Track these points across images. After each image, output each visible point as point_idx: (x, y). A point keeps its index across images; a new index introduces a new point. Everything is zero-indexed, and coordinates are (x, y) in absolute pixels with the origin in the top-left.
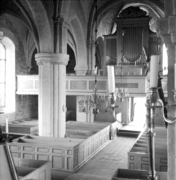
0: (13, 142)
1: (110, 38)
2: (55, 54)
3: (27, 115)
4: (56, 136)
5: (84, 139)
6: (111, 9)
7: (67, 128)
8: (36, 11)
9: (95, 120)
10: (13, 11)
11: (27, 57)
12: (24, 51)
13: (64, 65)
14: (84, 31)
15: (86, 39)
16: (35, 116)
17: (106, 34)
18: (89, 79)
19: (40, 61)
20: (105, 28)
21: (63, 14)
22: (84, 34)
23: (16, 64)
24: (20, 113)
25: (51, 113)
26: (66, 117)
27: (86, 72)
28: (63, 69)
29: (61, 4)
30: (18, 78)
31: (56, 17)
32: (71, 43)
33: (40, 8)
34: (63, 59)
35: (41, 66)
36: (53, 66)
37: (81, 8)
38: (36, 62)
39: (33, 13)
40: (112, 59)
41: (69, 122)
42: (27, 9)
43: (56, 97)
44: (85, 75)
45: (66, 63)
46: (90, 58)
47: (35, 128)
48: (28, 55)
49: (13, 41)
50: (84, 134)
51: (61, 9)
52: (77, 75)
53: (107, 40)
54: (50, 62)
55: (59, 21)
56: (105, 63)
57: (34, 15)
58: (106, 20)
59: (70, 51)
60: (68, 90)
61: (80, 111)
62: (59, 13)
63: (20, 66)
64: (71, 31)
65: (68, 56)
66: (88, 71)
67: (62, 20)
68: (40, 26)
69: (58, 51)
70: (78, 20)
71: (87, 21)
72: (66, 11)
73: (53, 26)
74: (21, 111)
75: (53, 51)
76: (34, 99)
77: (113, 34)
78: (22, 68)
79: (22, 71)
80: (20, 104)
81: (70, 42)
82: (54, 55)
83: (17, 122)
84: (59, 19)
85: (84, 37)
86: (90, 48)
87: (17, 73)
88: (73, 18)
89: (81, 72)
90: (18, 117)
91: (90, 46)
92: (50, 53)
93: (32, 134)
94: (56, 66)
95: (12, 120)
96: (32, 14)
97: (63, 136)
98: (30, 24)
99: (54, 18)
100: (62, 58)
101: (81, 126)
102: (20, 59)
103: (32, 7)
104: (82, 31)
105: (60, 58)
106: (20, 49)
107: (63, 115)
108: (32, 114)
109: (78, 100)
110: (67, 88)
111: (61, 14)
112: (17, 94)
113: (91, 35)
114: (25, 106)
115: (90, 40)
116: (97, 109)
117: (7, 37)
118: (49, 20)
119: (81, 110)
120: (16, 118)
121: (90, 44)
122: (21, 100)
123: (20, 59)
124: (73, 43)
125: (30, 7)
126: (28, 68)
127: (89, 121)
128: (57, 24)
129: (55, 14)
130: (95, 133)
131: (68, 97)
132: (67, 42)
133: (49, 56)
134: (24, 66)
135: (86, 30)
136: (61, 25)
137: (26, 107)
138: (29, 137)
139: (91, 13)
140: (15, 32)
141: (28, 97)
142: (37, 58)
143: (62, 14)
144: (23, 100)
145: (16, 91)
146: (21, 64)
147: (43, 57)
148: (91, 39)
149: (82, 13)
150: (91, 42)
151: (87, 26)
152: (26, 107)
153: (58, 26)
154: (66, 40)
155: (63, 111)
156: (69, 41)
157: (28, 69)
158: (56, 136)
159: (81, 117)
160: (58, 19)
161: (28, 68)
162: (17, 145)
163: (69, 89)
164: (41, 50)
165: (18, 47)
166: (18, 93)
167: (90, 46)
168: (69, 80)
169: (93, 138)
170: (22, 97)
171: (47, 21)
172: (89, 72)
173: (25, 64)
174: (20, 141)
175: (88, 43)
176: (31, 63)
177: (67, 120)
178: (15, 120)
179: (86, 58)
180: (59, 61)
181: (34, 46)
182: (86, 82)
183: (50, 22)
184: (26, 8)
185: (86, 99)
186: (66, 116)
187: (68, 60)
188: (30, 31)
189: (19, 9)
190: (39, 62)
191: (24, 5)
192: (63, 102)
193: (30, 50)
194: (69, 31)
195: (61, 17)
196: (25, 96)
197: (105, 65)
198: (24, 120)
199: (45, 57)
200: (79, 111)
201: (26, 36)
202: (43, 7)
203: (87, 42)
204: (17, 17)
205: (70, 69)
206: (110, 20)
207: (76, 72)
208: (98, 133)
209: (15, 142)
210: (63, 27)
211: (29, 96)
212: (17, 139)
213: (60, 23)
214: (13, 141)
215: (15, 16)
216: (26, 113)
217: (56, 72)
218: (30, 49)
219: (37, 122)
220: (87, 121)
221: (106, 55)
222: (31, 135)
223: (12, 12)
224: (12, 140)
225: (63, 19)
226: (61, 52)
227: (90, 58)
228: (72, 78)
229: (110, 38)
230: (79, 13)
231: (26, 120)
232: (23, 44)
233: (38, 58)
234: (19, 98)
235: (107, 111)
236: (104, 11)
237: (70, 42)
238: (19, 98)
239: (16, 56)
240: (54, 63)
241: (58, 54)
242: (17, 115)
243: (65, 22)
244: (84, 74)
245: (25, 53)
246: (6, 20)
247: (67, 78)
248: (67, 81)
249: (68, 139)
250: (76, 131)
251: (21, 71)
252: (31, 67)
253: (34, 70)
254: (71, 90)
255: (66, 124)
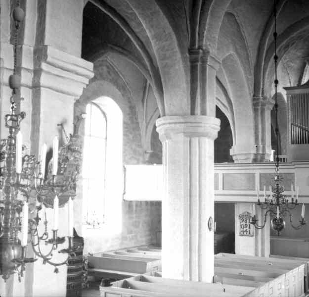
0: (112, 287)
1: (298, 92)
2: (192, 116)
3: (143, 240)
4: (195, 278)
5: (253, 287)
6: (299, 37)
7: (216, 265)
8: (158, 37)
9: (273, 252)
10: (119, 47)
11: (143, 133)
12: (138, 123)
13: (209, 137)
14: (248, 79)
15: (252, 95)
16: (156, 243)
17: (288, 85)
18: (257, 171)
19: (165, 131)
20: (287, 77)
21: (208, 43)
22: (248, 85)
23: (125, 145)
24: (130, 235)
25: (186, 231)
26: (215, 246)
27: (252, 157)
28: (208, 148)
29: (205, 24)
30: (127, 169)
31: (195, 49)
32: (223, 105)
33: (164, 31)
34: (208, 125)
35: (167, 141)
36: (189, 139)
37: (242, 38)
38: (157, 134)
39: (153, 42)
40: (301, 130)
41: (220, 255)
42: (141, 37)
43: (196, 199)
44: (251, 162)
45: (215, 134)
46: (260, 130)
47: (155, 263)
48: (145, 130)
49: (119, 105)
50: (251, 279)
51: (203, 33)
52: (235, 162)
53: (293, 98)
54: (184, 133)
55: (200, 55)
56: (290, 140)
57: (154, 47)
58: (289, 63)
59: (219, 114)
60: (217, 192)
61: (242, 233)
62: (201, 40)
63: (132, 148)
64: (221, 80)
65: (218, 121)
66: (256, 155)
67: (206, 53)
68: (166, 66)
69: (198, 110)
70: (236, 57)
71: (253, 61)
72: (214, 37)
73: (189, 64)
74: (131, 232)
75: (189, 111)
76: (155, 208)
77: (305, 84)
78: (135, 151)
79: (135, 159)
80: (130, 218)
81: (222, 103)
82: (191, 119)
83: (124, 251)
84: (201, 51)
85: (247, 90)
86: (260, 111)
87: (126, 161)
88: (227, 54)
89: (243, 157)
90: (125, 242)
91: (259, 107)
92: (183, 115)
93: (149, 273)
94: (195, 141)
95: (114, 249)
96: (151, 44)
97: (211, 280)
98: (147, 63)
99: (192, 51)
100: (207, 123)
101: (245, 264)
102: (131, 136)
103: (150, 31)
104: (245, 80)
105: (203, 125)
106: (131, 118)
107: (209, 239)
108: (152, 240)
109: (239, 211)
110: (216, 188)
111: (204, 43)
112: (124, 200)
113: (261, 87)
114: (139, 222)
115: (259, 96)
116: (281, 220)
117: (108, 96)
118: (182, 53)
119: (244, 232)
120: (122, 244)
121: (260, 104)
122: (132, 211)
123: (131, 136)
124: (226, 104)
125: (147, 31)
126: (146, 152)
127: (260, 255)
128: (198, 61)
129: (193, 43)
130: (275, 276)
131: (219, 206)
132: (217, 103)
133: (182, 120)
134: (138, 149)
135: (252, 77)
136: (204, 62)
137: (141, 226)
138: (143, 279)
139: (260, 50)
140: (122, 88)
141: (144, 206)
142: (160, 125)
143: (205, 42)
144: (136, 210)
145: (124, 194)
146: (134, 147)
147: (170, 123)
148: (261, 95)
149: (245, 47)
150: (261, 100)
151: (252, 71)
152: (141, 226)
153: (199, 64)
154: (213, 99)
155: (210, 229)
156: (219, 100)
157: (145, 155)
158: (195, 278)
159: (244, 245)
160: (199, 52)
161: (146, 152)
162: (118, 292)
163: (221, 191)
164: (167, 111)
165: (129, 114)
166: (128, 198)
167: (259, 107)
168: (220, 173)
169: (270, 287)
170: (134, 204)
171: (179, 55)
172: (259, 157)
173: (140, 146)
174: (126, 285)
175: (255, 102)
176: (150, 143)
177: (217, 251)
178: (119, 248)
179: (253, 131)
180: (200, 130)
181: (156, 113)
182: (254, 174)
183: (184, 58)
184: (139, 35)
185: (254, 214)
186: (215, 243)
187: (219, 128)
188: (149, 82)
189: (128, 39)
190: (163, 132)
191: (136, 30)
192: (209, 212)
193: (150, 120)
194: (219, 81)
195: (204, 48)
196: (139, 204)
197: (290, 143)
198: (136, 249)
199: (175, 123)
200: (240, 233)
201: (142, 94)
202: (170, 29)
203: (254, 100)
204: (126, 56)
205: (222, 154)
206: (296, 63)
207: (234, 158)
208: (281, 276)
209: (116, 286)
210: (207, 65)
211: (147, 202)
212: (121, 282)
213: (202, 58)
214: (112, 285)
215: (122, 53)
216: (141, 237)
217: (196, 149)
218: (149, 119)
219: (159, 253)
220: (256, 255)
221: (292, 124)
222: (145, 276)
223: (116, 48)
224: (111, 283)
225: (208, 52)
226: (203, 113)
227: (260, 130)
228: (224, 169)
229: (298, 92)
230: (238, 47)
231: (140, 248)
232: (137, 110)
233: (161, 127)
234: (129, 206)
235: (305, 224)
236: (285, 42)
237: (222, 103)
238: (129, 206)
239: (124, 132)
240: (192, 135)
241: (198, 116)
242: (124, 238)
243: (209, 65)
244: (250, 161)
245: (140, 126)
246: (108, 67)
247: (217, 168)
248: (216, 175)
249: (219, 286)
250: (236, 271)
251: (133, 157)
252: (150, 151)
253: (156, 157)
254: (226, 192)
255: (215, 258)
